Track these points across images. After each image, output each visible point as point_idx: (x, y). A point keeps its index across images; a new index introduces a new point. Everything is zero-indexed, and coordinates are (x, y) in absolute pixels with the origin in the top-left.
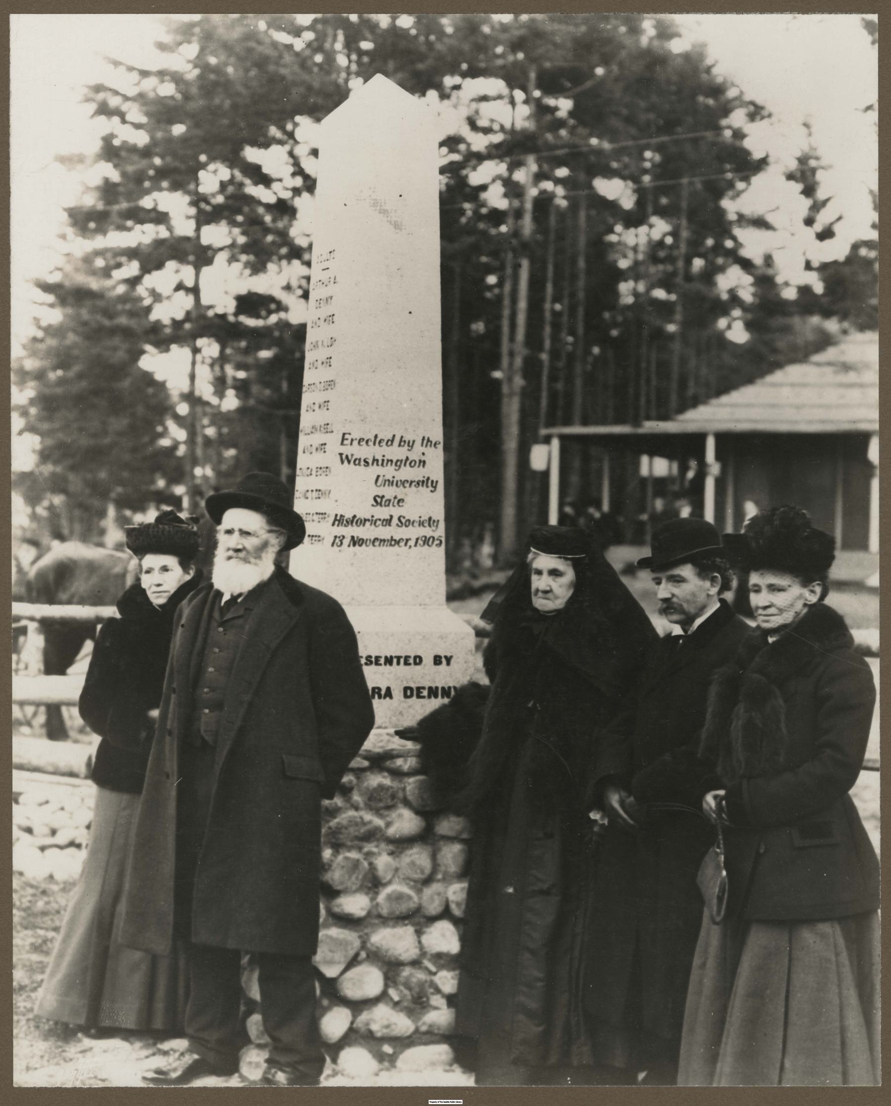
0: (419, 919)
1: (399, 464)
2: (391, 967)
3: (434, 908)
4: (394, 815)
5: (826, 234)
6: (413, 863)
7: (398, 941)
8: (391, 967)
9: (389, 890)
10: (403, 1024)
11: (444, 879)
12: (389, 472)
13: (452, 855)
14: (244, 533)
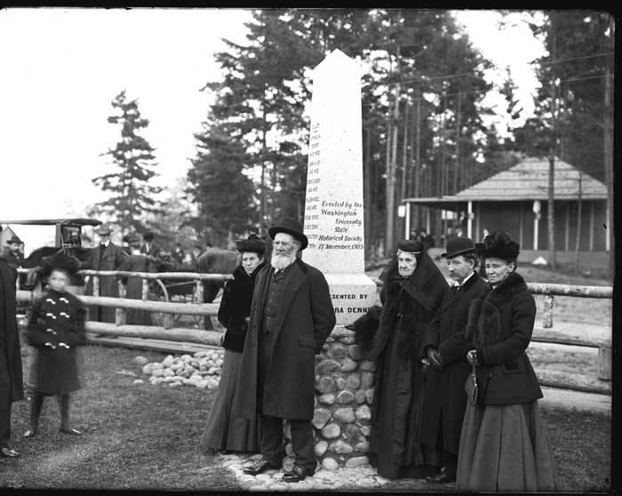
0: (354, 404)
1: (346, 214)
2: (343, 425)
3: (360, 400)
5: (516, 116)
6: (351, 381)
7: (346, 413)
9: (342, 392)
10: (348, 448)
12: (341, 217)
13: (368, 377)
14: (284, 243)
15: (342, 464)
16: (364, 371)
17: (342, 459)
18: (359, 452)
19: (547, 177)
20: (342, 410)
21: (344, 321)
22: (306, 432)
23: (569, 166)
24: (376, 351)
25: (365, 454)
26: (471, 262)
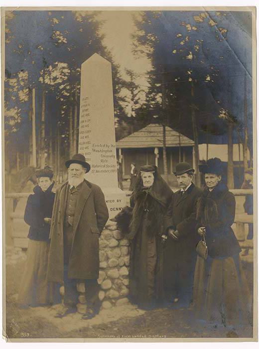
0: (118, 267)
1: (106, 152)
2: (112, 279)
3: (122, 264)
4: (111, 240)
5: (136, 103)
6: (116, 253)
7: (114, 273)
8: (112, 279)
9: (111, 260)
10: (117, 294)
11: (123, 256)
12: (104, 153)
13: (125, 250)
14: (77, 170)
15: (114, 304)
16: (122, 246)
17: (113, 301)
18: (123, 295)
19: (162, 135)
20: (111, 271)
21: (112, 215)
22: (93, 287)
23: (171, 129)
24: (132, 234)
25: (126, 296)
26: (191, 177)
